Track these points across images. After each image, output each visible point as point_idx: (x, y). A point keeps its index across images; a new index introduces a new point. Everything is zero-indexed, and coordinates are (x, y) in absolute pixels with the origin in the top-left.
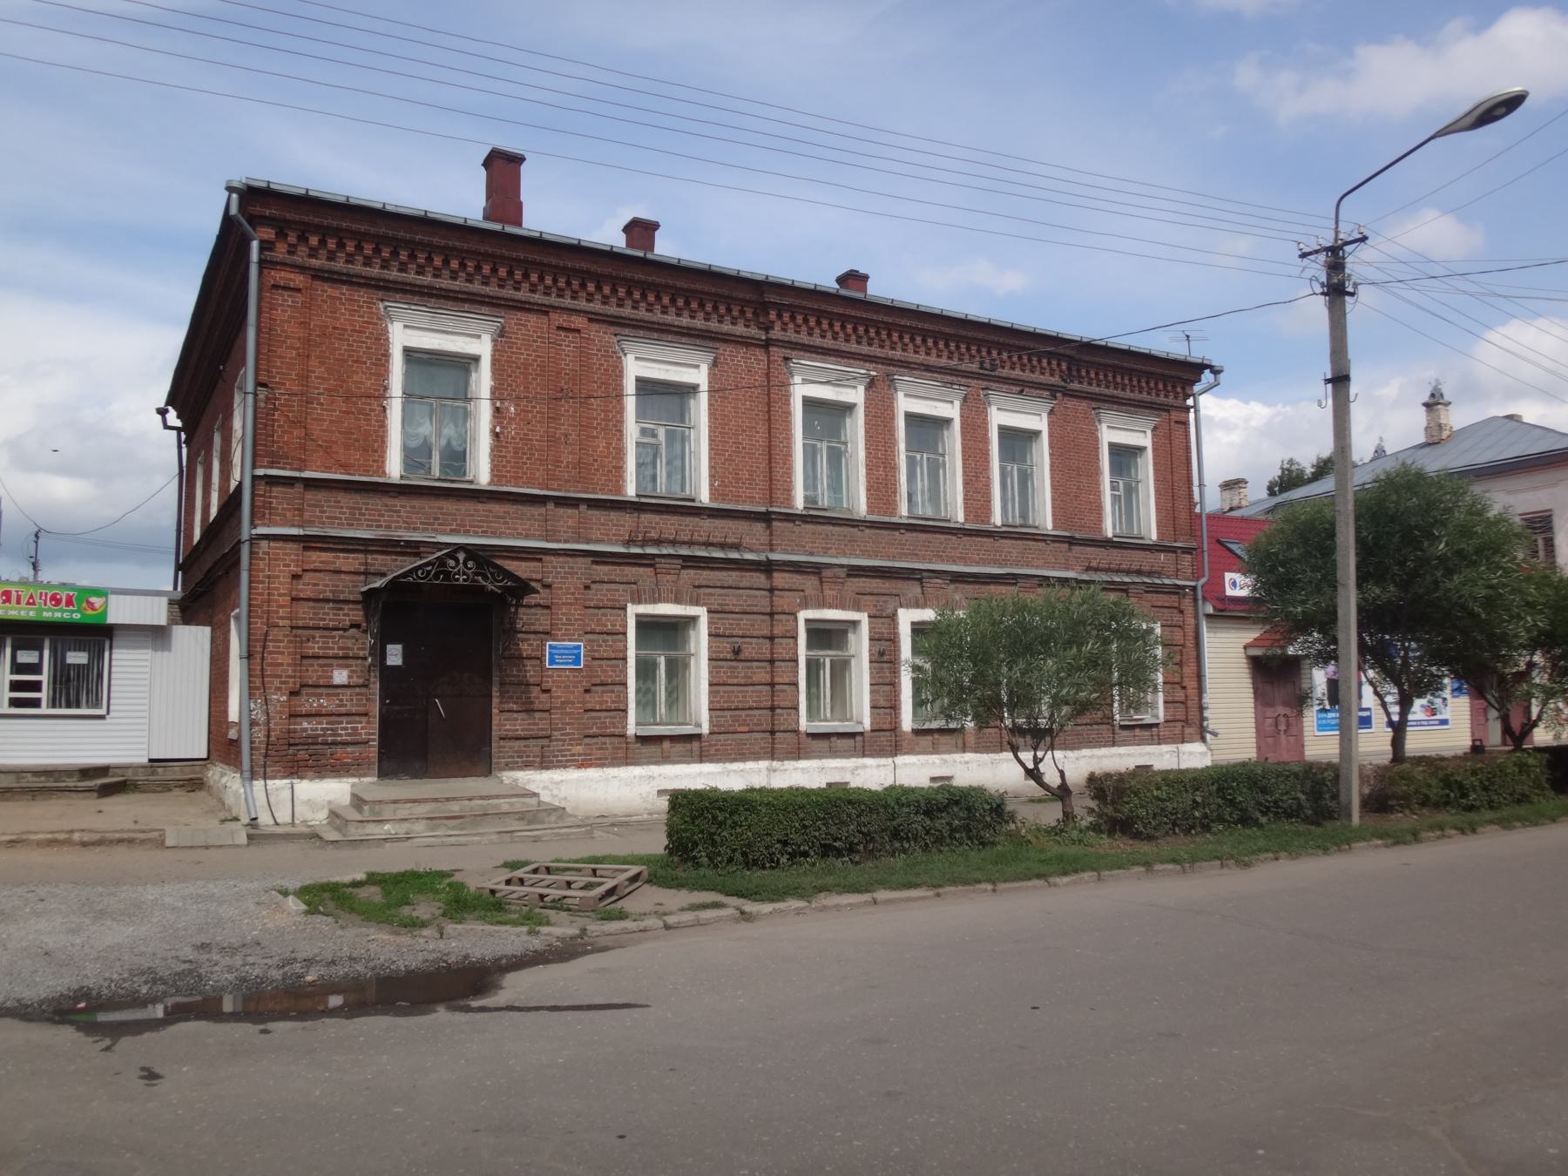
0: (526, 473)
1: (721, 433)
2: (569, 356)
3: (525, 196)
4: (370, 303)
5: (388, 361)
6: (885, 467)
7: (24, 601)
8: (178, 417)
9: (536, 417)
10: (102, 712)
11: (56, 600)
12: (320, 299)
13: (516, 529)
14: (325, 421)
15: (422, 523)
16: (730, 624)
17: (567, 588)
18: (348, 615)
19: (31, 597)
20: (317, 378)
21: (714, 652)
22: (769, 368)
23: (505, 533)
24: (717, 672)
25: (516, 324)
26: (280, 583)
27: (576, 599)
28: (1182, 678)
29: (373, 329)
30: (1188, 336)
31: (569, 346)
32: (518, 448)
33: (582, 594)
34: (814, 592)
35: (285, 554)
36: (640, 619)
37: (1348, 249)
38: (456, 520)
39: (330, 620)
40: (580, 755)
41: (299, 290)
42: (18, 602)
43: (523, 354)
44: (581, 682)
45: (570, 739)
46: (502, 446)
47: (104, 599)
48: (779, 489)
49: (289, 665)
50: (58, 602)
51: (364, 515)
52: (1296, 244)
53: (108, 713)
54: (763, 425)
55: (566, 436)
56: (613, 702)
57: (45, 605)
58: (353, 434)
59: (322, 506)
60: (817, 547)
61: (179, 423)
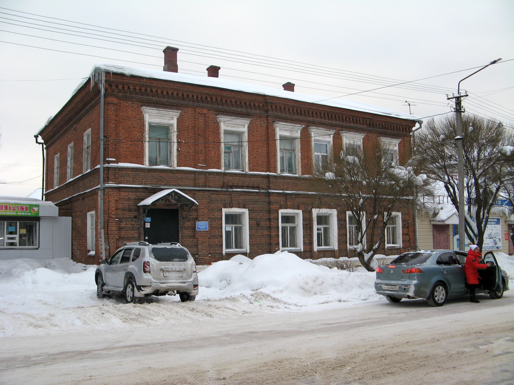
0: (188, 164)
1: (252, 148)
2: (202, 123)
3: (178, 63)
4: (138, 107)
5: (144, 127)
6: (308, 159)
7: (12, 209)
8: (42, 139)
9: (191, 144)
10: (37, 247)
11: (22, 209)
12: (122, 107)
13: (186, 183)
14: (124, 148)
15: (155, 182)
16: (256, 215)
17: (202, 203)
18: (133, 213)
19: (14, 208)
20: (121, 133)
21: (251, 224)
22: (268, 125)
23: (182, 184)
24: (252, 231)
25: (184, 113)
26: (112, 203)
27: (205, 207)
28: (408, 231)
29: (139, 116)
30: (409, 104)
31: (202, 120)
32: (186, 155)
33: (208, 205)
34: (284, 203)
35: (113, 193)
36: (226, 213)
37: (462, 98)
38: (166, 180)
39: (128, 215)
40: (208, 260)
41: (116, 104)
42: (10, 210)
43: (187, 123)
44: (207, 235)
45: (204, 255)
46: (180, 155)
47: (38, 208)
48: (272, 167)
49: (115, 230)
50: (23, 209)
51: (137, 179)
52: (446, 95)
53: (39, 247)
54: (266, 145)
55: (201, 151)
56: (218, 242)
57: (19, 210)
58: (133, 152)
59: (124, 177)
60: (285, 187)
61: (42, 141)
